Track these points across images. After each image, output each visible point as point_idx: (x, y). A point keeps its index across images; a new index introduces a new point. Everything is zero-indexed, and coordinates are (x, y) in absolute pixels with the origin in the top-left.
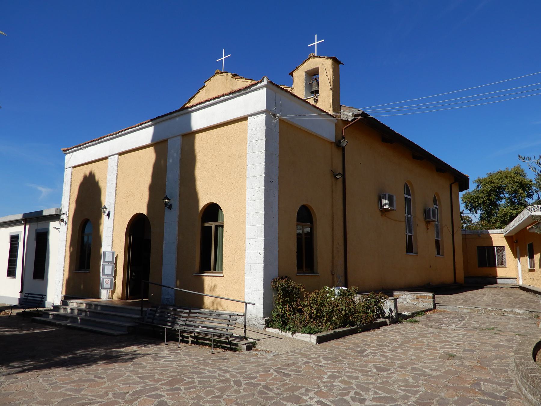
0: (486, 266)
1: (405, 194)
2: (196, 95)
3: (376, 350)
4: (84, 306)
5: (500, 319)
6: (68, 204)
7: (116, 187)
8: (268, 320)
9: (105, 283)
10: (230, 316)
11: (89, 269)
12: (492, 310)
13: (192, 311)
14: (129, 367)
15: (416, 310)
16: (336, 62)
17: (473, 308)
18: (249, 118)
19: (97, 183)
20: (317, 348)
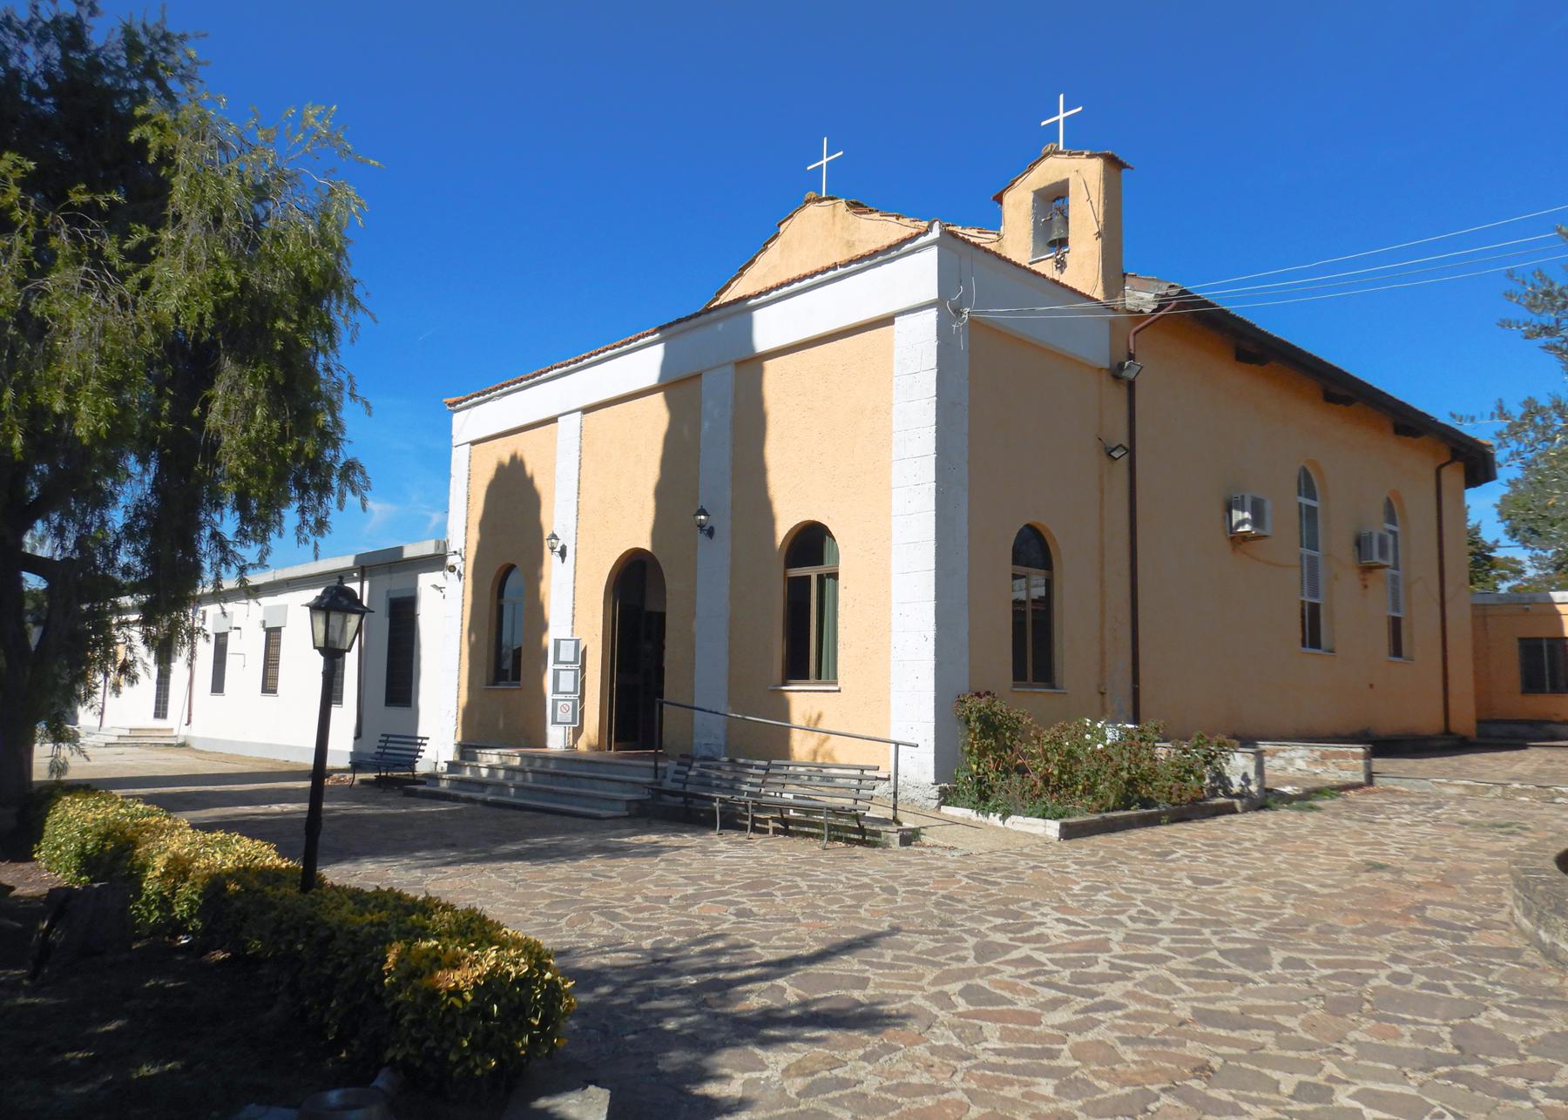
0: (1543, 692)
1: (1300, 495)
2: (756, 257)
3: (1197, 852)
4: (517, 762)
5: (1542, 809)
6: (464, 531)
7: (579, 489)
8: (946, 789)
9: (559, 712)
10: (862, 770)
11: (519, 680)
12: (1523, 790)
13: (773, 762)
14: (657, 864)
15: (1316, 785)
16: (1113, 163)
17: (1472, 783)
18: (896, 319)
19: (531, 480)
20: (1060, 847)
